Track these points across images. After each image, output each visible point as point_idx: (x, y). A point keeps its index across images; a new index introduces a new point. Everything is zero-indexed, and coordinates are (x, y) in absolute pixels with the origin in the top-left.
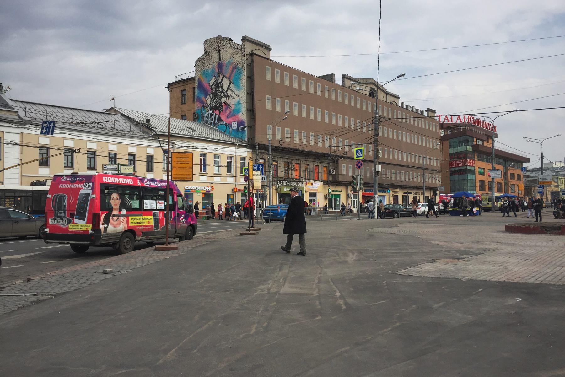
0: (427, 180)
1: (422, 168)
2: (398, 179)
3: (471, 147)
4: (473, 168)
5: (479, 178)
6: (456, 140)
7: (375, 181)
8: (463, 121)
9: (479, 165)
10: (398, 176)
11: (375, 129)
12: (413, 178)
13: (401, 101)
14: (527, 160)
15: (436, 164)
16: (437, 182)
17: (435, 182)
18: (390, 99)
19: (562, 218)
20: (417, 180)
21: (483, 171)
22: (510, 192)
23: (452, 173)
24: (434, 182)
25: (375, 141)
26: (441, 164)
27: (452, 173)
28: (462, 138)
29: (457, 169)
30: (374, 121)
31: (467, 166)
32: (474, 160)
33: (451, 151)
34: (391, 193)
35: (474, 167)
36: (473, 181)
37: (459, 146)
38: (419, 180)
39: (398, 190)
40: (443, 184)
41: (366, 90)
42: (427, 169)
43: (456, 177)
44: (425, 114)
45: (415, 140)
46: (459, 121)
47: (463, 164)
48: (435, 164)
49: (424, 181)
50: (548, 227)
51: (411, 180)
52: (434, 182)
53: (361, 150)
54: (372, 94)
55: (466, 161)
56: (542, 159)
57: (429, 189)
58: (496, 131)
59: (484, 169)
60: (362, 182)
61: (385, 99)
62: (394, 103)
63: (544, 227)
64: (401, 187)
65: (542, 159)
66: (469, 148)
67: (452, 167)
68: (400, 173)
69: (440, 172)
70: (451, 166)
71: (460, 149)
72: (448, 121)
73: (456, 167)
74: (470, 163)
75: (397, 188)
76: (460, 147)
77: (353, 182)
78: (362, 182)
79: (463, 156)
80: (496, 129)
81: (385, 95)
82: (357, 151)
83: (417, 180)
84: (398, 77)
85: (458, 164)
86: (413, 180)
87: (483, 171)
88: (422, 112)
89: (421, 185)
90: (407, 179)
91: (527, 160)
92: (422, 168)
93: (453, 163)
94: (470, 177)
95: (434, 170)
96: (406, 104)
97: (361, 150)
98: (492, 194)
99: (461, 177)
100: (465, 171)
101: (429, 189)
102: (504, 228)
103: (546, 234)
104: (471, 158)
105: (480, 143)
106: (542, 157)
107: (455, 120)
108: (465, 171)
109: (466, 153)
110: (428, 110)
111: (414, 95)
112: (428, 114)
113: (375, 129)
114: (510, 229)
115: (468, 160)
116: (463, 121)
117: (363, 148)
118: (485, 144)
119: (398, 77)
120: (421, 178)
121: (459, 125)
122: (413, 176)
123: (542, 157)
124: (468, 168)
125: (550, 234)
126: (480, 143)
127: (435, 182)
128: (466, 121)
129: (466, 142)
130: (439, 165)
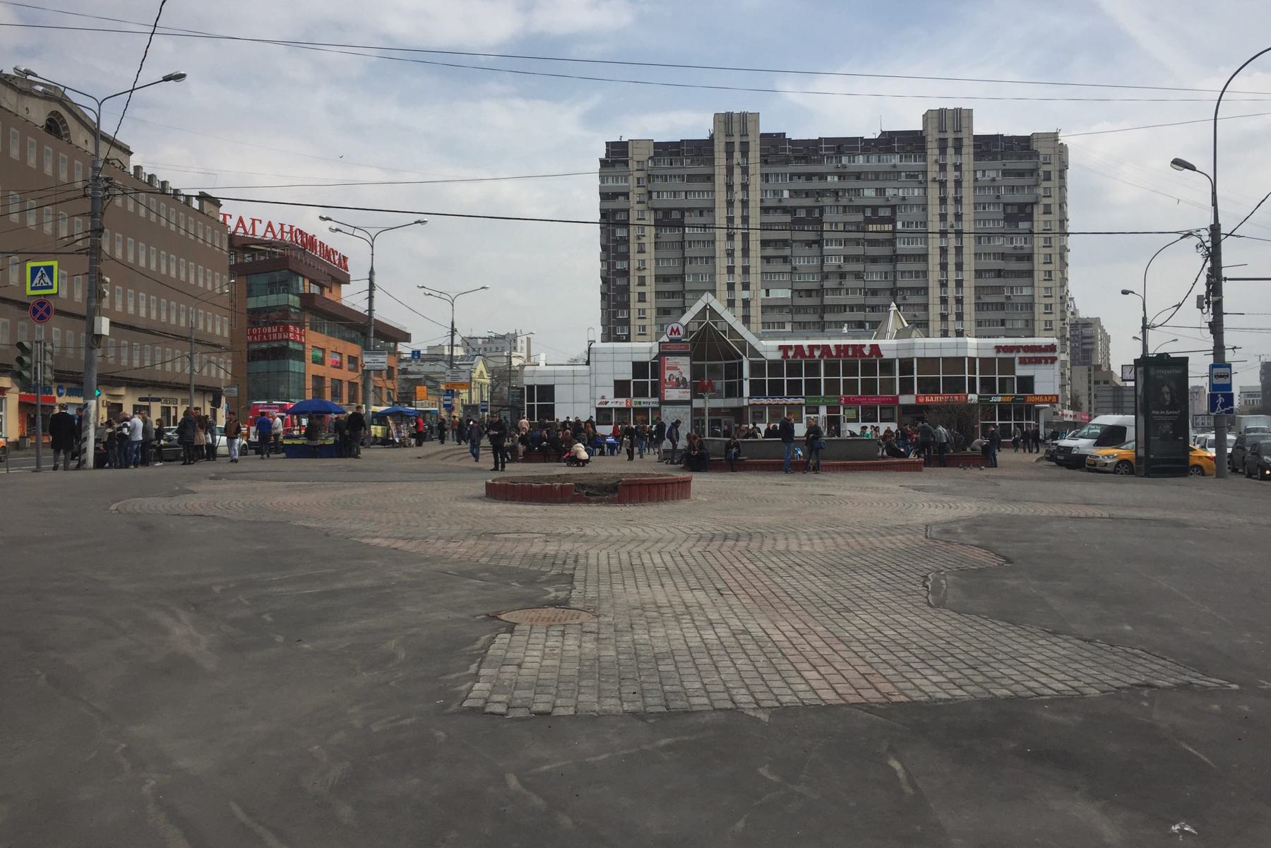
0: (197, 369)
1: (186, 339)
2: (124, 362)
3: (297, 298)
4: (299, 347)
5: (313, 370)
6: (263, 279)
7: (89, 362)
8: (279, 237)
9: (314, 340)
10: (124, 353)
11: (93, 215)
12: (163, 363)
13: (134, 161)
14: (406, 337)
15: (219, 328)
16: (222, 373)
17: (218, 373)
18: (114, 153)
19: (522, 461)
20: (173, 367)
21: (320, 354)
22: (746, 392)
23: (254, 356)
24: (213, 373)
25: (92, 247)
26: (231, 331)
27: (254, 356)
28: (278, 276)
29: (264, 346)
30: (89, 191)
31: (288, 340)
32: (302, 326)
33: (253, 303)
34: (103, 397)
35: (303, 344)
36: (302, 375)
37: (272, 293)
38: (178, 369)
39: (122, 391)
40: (235, 380)
41: (38, 113)
42: (198, 341)
43: (262, 365)
44: (195, 204)
45: (173, 269)
46: (269, 235)
47: (280, 337)
48: (218, 331)
49: (192, 370)
50: (590, 487)
51: (158, 367)
52: (213, 373)
53: (49, 270)
54: (54, 126)
55: (287, 330)
56: (452, 336)
57: (203, 390)
58: (346, 268)
59: (323, 350)
60: (49, 361)
61: (91, 148)
62: (118, 164)
63: (583, 486)
64: (132, 384)
65: (452, 336)
66: (294, 300)
67: (253, 342)
68: (130, 347)
69: (227, 350)
70: (250, 338)
71: (273, 300)
72: (246, 232)
73: (262, 341)
74: (295, 334)
75: (119, 385)
76: (274, 296)
77: (20, 360)
78: (49, 361)
79: (281, 317)
80: (349, 263)
81: (91, 139)
82: (35, 271)
83: (173, 367)
84: (167, 79)
85: (267, 334)
86: (163, 368)
87: (321, 358)
88: (188, 197)
89: (184, 380)
90: (147, 363)
91: (406, 337)
92: (186, 339)
93: (255, 331)
94: (294, 365)
95: (214, 346)
96: (147, 170)
97: (49, 270)
98: (367, 408)
99: (273, 365)
100: (282, 353)
101: (203, 390)
102: (483, 492)
103: (588, 502)
104: (296, 324)
105: (315, 289)
106: (453, 331)
107: (260, 231)
108: (282, 353)
109: (285, 310)
110: (203, 197)
111: (170, 155)
112: (201, 205)
113: (93, 215)
114: (496, 492)
115: (292, 328)
116: (279, 237)
117: (55, 264)
118: (327, 295)
119: (167, 79)
120: (182, 363)
121: (269, 244)
122: (163, 357)
123: (453, 331)
124: (291, 345)
125: (596, 502)
126: (315, 289)
127: (218, 373)
128: (287, 237)
129: (286, 286)
130: (226, 334)
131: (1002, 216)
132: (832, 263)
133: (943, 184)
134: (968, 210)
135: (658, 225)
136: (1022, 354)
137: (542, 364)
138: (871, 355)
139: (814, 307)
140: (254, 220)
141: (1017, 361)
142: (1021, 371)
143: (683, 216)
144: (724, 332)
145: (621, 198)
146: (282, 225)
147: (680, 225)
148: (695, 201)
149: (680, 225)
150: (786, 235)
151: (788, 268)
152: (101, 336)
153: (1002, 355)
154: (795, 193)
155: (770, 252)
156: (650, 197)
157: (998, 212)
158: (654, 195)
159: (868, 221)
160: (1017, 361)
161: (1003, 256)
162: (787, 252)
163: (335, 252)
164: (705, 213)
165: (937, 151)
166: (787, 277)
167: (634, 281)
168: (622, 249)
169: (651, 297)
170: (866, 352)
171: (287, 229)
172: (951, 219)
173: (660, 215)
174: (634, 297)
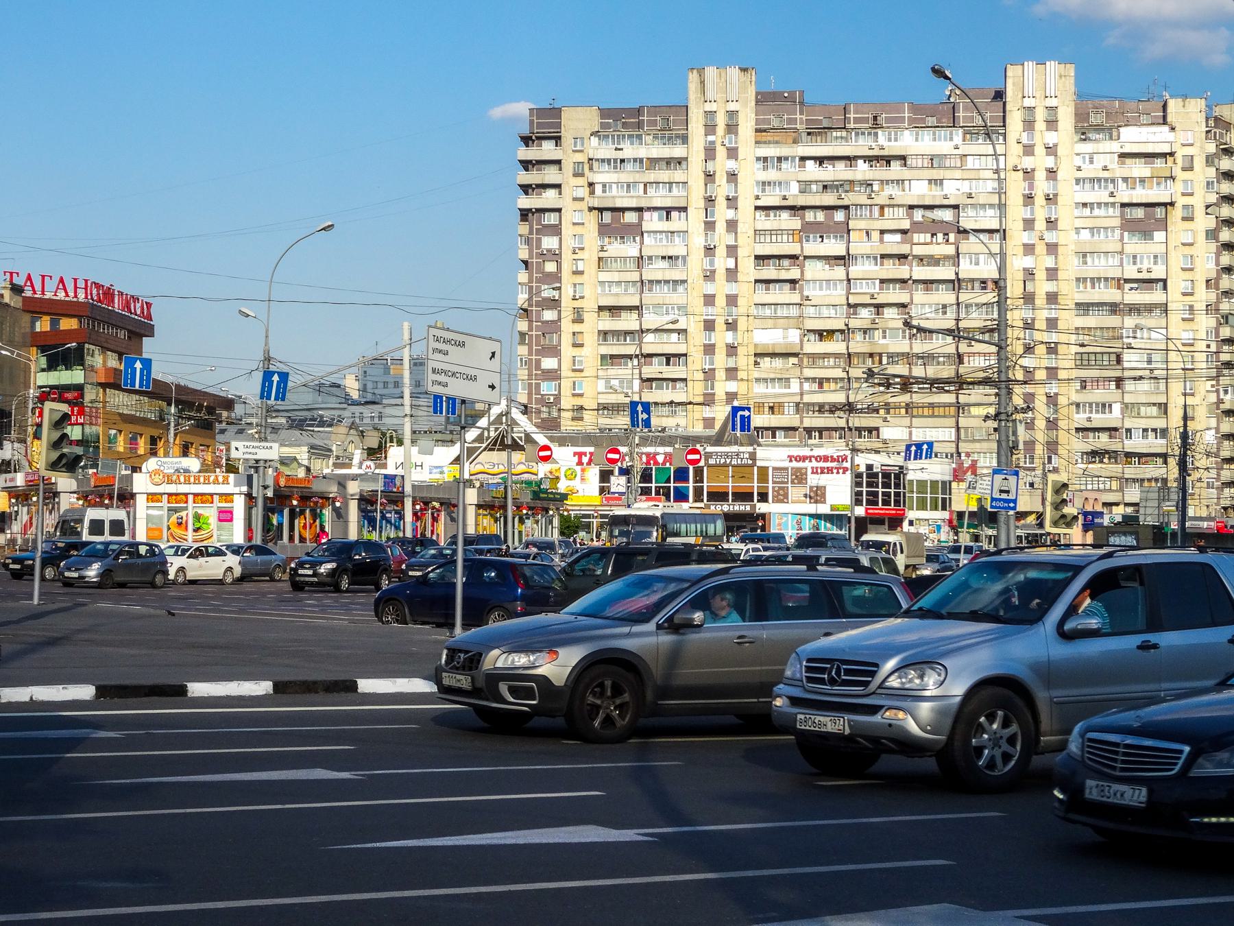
46: (61, 295)
131: (1116, 222)
132: (864, 291)
133: (1028, 174)
134: (1066, 214)
135: (604, 230)
136: (814, 464)
137: (190, 540)
138: (664, 463)
139: (836, 356)
140: (43, 277)
141: (809, 471)
142: (813, 480)
143: (641, 219)
144: (520, 438)
145: (551, 193)
146: (75, 280)
147: (636, 231)
148: (659, 198)
149: (636, 231)
150: (794, 249)
151: (796, 298)
152: (1150, 800)
153: (795, 464)
154: (805, 186)
155: (770, 272)
156: (592, 193)
157: (1112, 218)
158: (598, 189)
159: (917, 227)
160: (809, 471)
161: (1121, 282)
162: (794, 273)
163: (135, 299)
164: (674, 214)
165: (1020, 126)
166: (794, 311)
167: (567, 316)
168: (550, 267)
169: (590, 339)
170: (660, 459)
171: (81, 284)
172: (1040, 225)
173: (159, 579)
174: (566, 340)
